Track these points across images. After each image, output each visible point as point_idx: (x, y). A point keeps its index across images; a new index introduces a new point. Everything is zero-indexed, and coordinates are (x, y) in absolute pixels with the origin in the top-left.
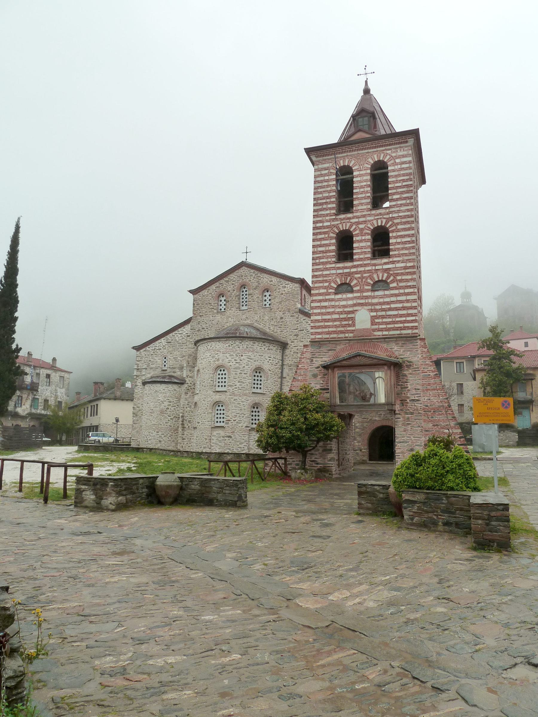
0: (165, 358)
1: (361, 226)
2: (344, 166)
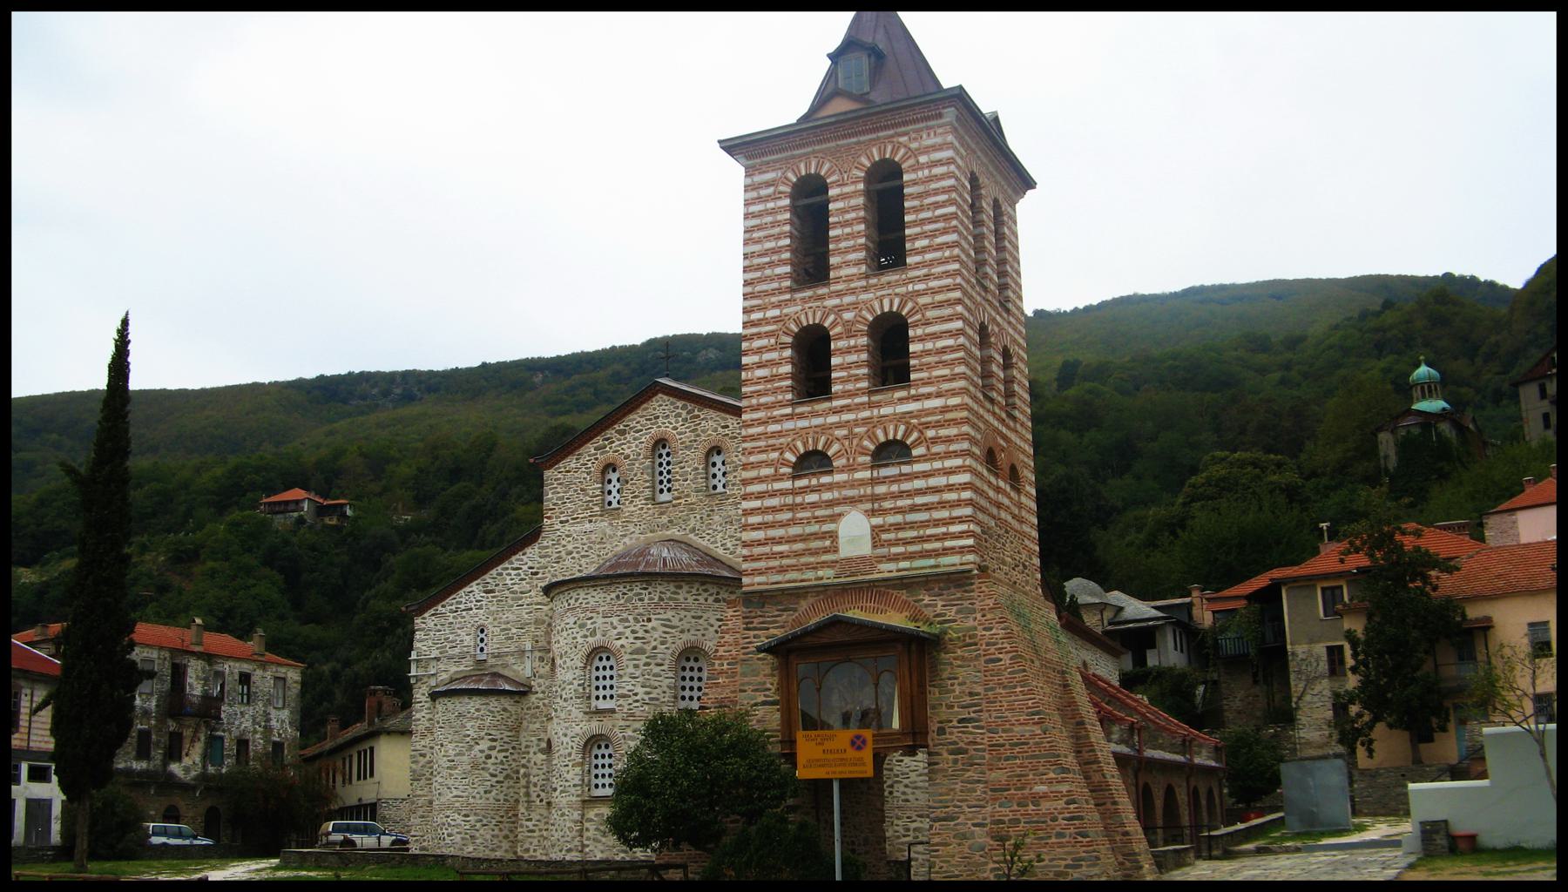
0: (482, 631)
1: (848, 316)
2: (809, 176)
